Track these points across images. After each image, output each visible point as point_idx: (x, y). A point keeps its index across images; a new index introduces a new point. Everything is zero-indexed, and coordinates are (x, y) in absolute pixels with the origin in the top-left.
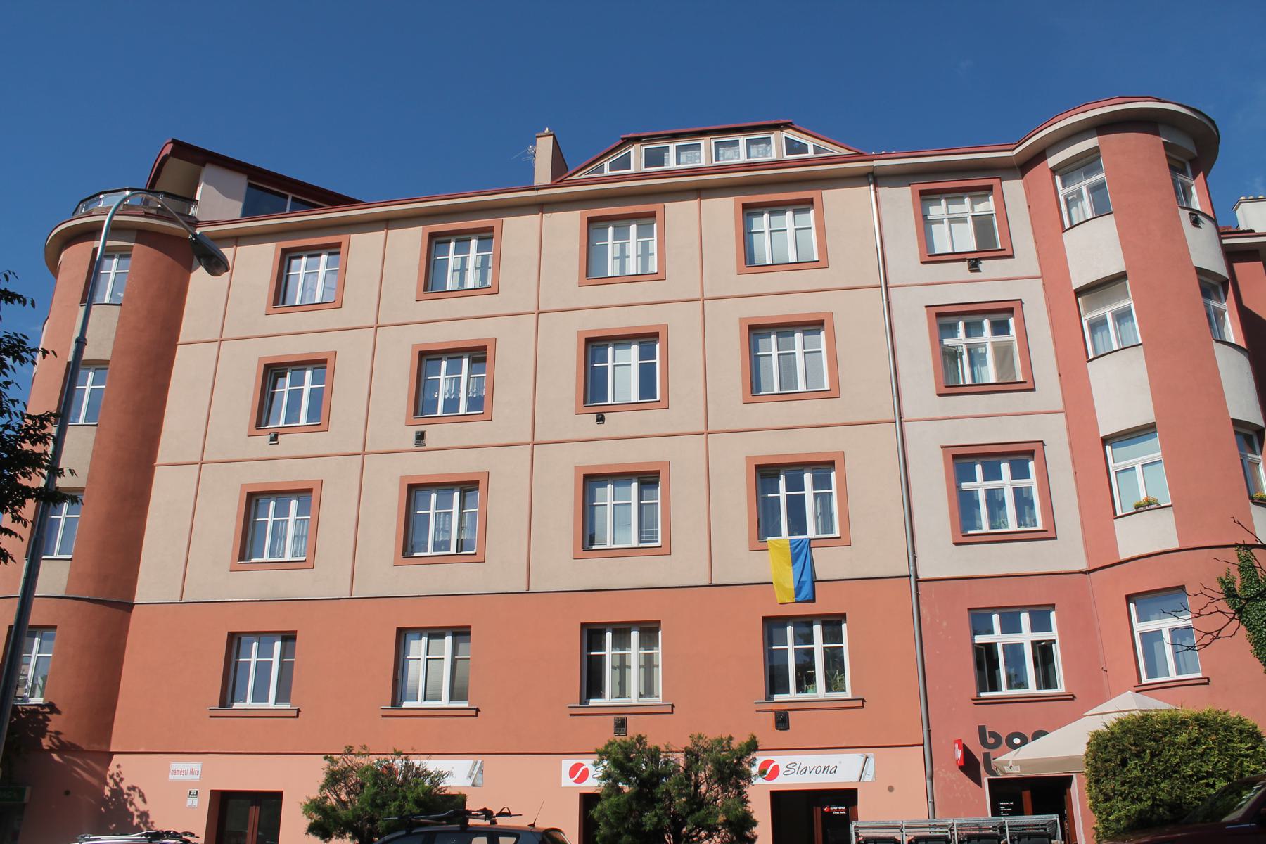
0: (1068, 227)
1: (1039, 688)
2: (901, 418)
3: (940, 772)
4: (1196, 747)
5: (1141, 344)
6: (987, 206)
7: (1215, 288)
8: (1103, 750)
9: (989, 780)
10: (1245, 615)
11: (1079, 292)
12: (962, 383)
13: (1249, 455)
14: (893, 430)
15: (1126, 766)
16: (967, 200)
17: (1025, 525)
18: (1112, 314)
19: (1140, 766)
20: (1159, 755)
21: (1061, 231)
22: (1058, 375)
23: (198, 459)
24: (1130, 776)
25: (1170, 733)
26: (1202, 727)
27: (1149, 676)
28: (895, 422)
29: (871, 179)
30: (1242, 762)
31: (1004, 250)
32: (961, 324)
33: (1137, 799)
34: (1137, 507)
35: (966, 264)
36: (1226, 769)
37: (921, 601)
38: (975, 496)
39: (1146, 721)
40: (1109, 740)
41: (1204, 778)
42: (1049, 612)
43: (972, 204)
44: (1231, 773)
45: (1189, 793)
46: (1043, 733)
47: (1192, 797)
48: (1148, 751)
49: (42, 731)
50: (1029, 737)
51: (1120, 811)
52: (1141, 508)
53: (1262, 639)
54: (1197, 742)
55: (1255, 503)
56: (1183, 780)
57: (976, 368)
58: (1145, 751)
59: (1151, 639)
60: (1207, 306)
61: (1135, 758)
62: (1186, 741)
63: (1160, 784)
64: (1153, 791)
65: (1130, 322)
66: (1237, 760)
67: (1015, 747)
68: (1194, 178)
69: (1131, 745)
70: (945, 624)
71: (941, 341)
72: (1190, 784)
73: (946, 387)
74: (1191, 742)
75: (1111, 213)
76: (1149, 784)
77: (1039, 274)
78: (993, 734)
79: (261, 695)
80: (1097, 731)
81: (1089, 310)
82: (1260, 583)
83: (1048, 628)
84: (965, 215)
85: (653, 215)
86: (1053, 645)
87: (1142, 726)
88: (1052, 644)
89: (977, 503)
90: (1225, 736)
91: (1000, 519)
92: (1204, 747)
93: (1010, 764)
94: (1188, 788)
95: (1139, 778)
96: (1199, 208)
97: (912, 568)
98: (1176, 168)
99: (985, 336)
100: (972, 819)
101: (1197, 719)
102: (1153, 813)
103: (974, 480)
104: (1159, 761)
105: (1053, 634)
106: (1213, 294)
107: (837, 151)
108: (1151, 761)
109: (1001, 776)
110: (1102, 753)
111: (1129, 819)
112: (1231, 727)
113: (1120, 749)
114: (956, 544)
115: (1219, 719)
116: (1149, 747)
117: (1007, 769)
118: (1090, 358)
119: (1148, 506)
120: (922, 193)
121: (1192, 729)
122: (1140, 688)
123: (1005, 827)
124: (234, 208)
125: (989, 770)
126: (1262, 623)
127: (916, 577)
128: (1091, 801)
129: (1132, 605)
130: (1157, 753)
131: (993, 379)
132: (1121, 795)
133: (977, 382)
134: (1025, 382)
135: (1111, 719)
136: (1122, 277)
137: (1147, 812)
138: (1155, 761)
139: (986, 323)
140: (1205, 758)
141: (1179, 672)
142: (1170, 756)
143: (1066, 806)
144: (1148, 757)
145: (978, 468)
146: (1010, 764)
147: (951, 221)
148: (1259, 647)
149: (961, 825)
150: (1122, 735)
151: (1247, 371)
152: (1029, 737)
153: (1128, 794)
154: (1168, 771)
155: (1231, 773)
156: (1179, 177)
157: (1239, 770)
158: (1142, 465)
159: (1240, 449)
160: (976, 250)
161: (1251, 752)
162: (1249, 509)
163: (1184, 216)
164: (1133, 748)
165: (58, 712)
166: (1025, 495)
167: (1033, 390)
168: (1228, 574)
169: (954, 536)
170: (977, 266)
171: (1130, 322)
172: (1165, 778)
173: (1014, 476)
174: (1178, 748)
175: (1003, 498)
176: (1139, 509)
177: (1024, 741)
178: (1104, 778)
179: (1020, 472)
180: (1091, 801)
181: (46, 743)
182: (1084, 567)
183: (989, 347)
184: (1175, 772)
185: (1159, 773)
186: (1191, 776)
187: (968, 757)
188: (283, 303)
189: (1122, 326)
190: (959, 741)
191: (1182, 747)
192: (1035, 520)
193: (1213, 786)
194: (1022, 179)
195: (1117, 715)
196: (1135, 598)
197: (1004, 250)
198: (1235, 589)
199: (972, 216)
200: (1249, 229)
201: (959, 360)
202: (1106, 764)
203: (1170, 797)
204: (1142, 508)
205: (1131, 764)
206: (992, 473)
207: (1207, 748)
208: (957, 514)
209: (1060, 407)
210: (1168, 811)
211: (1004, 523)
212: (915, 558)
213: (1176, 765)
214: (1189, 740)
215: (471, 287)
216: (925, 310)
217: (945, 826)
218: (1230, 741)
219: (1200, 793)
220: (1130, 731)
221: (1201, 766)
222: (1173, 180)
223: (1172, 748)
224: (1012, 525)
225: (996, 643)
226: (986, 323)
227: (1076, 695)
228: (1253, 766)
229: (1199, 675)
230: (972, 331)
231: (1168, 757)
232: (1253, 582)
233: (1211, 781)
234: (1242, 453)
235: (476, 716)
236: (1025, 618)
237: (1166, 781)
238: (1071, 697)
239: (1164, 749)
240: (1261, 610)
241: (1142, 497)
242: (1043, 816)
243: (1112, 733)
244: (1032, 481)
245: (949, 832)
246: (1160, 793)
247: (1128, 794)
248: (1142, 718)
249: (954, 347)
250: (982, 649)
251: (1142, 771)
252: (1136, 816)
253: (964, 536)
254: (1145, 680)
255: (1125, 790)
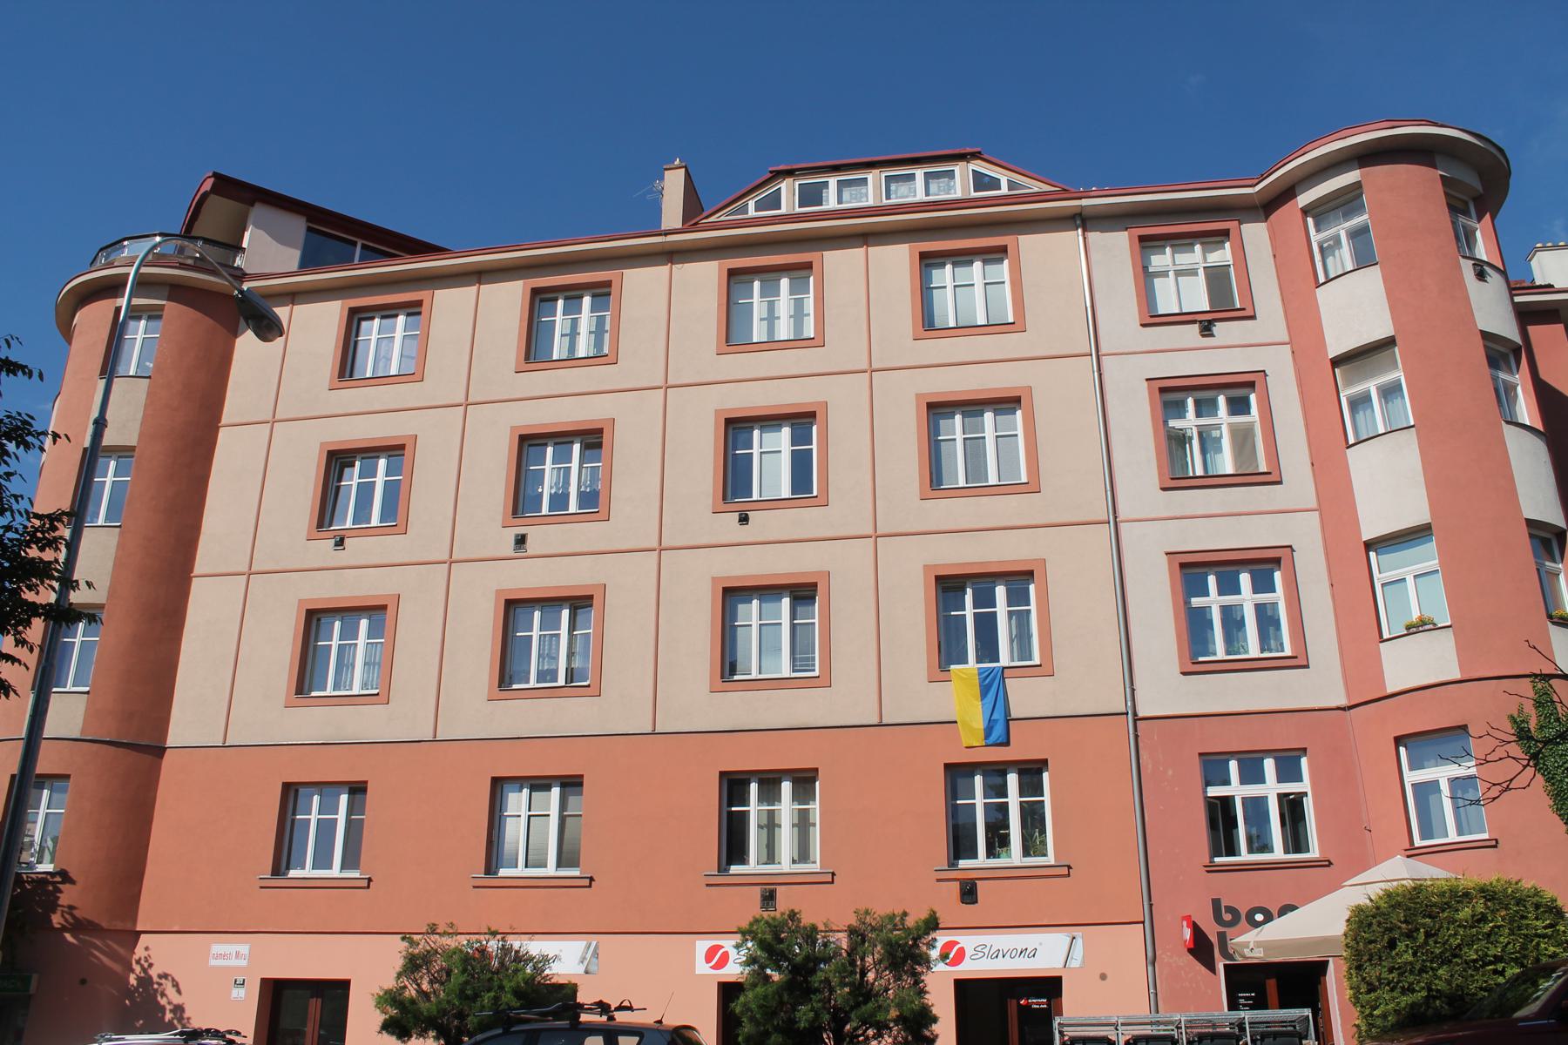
0: (1323, 281)
1: (1286, 851)
2: (1116, 517)
3: (1164, 956)
4: (1481, 925)
5: (1413, 426)
6: (1223, 255)
7: (1505, 357)
8: (1366, 929)
9: (1225, 966)
10: (1541, 761)
11: (1336, 362)
12: (1191, 475)
13: (1547, 563)
14: (1106, 532)
15: (1395, 948)
16: (1198, 248)
17: (1270, 650)
18: (1377, 388)
19: (1412, 948)
20: (1435, 934)
21: (1314, 286)
22: (1310, 465)
23: (245, 569)
24: (1400, 961)
25: (1450, 907)
26: (1489, 900)
27: (1423, 838)
28: (1109, 523)
29: (1078, 222)
30: (1538, 944)
31: (1244, 309)
32: (1190, 402)
33: (1408, 989)
34: (1408, 628)
35: (1196, 326)
36: (1519, 952)
37: (1140, 745)
38: (1208, 614)
39: (1419, 893)
40: (1374, 917)
41: (1491, 963)
42: (1300, 758)
43: (1204, 252)
44: (1525, 957)
45: (1473, 982)
46: (1292, 908)
47: (1476, 987)
48: (1422, 930)
49: (53, 906)
50: (1275, 913)
51: (1387, 1004)
52: (1414, 629)
53: (1563, 791)
54: (1483, 919)
55: (1554, 623)
56: (1465, 966)
57: (1208, 456)
58: (1419, 930)
59: (1426, 791)
60: (1495, 379)
61: (1406, 939)
62: (1469, 917)
63: (1437, 970)
64: (1427, 979)
65: (1399, 398)
66: (1532, 941)
67: (1257, 925)
68: (1479, 221)
69: (1401, 922)
70: (1170, 772)
71: (1165, 422)
72: (1474, 970)
73: (1172, 479)
74: (1476, 918)
75: (1377, 264)
76: (1423, 970)
77: (1287, 339)
78: (1230, 909)
79: (323, 860)
80: (1359, 905)
81: (1349, 383)
82: (1560, 722)
83: (1298, 778)
84: (1196, 266)
85: (808, 266)
86: (1305, 799)
87: (1415, 898)
88: (1302, 798)
89: (1211, 622)
90: (1517, 912)
91: (1238, 643)
92: (1491, 925)
93: (1251, 946)
94: (1472, 976)
95: (1411, 963)
96: (1485, 258)
97: (1129, 704)
98: (1456, 208)
99: (1220, 416)
100: (1204, 1014)
101: (1482, 890)
102: (1428, 1007)
103: (1207, 594)
104: (1436, 942)
105: (1305, 786)
106: (1502, 364)
107: (1036, 187)
108: (1426, 943)
109: (1240, 961)
110: (1365, 932)
111: (1398, 1014)
112: (1525, 901)
113: (1387, 927)
114: (1184, 674)
115: (1510, 891)
116: (1424, 925)
117: (1247, 952)
118: (1350, 443)
119: (1422, 626)
120: (1142, 239)
121: (1477, 903)
122: (1412, 852)
123: (1245, 1023)
124: (290, 257)
125: (1225, 954)
126: (1563, 771)
127: (1135, 714)
128: (1352, 992)
129: (1402, 750)
130: (1433, 932)
131: (1229, 470)
132: (1388, 984)
133: (1210, 473)
134: (1269, 473)
135: (1375, 891)
136: (1389, 342)
137: (1420, 1005)
138: (1431, 942)
139: (1222, 400)
140: (1493, 938)
141: (1460, 833)
142: (1449, 936)
143: (1320, 998)
144: (1421, 937)
145: (1212, 580)
146: (1251, 946)
147: (1178, 273)
148: (1560, 801)
149: (1190, 1021)
150: (1390, 910)
151: (1544, 460)
152: (1275, 913)
153: (1398, 983)
154: (1447, 955)
155: (1525, 957)
156: (1460, 219)
157: (1534, 954)
158: (1415, 576)
159: (1536, 556)
160: (1208, 309)
161: (1549, 931)
162: (1547, 630)
163: (1467, 267)
164: (1404, 926)
165: (72, 882)
166: (1269, 613)
167: (1280, 483)
168: (1520, 711)
169: (1181, 664)
170: (1210, 330)
171: (1399, 398)
172: (1443, 963)
173: (1256, 589)
174: (1459, 926)
175: (1243, 617)
176: (1411, 630)
177: (1269, 918)
178: (1367, 964)
179: (1263, 584)
180: (1352, 992)
181: (56, 919)
182: (1343, 702)
183: (1225, 429)
184: (1455, 956)
185: (1435, 957)
186: (1475, 961)
187: (1199, 937)
188: (351, 376)
189: (1390, 403)
190: (1188, 918)
191: (1463, 925)
192: (1282, 644)
193: (1502, 973)
194: (1266, 221)
195: (1383, 885)
196: (1406, 740)
197: (1244, 309)
198: (1529, 729)
199: (1204, 268)
200: (1547, 283)
201: (1187, 446)
202: (1370, 946)
203: (1449, 987)
204: (1415, 630)
205: (1401, 946)
206: (1229, 586)
207: (1495, 927)
208: (1185, 637)
209: (1313, 504)
210: (1446, 1004)
211: (1243, 647)
212: (1133, 690)
213: (1456, 948)
214: (1473, 916)
215: (583, 356)
216: (1146, 384)
217: (1171, 1023)
218: (1523, 917)
219: (1486, 982)
220: (1399, 905)
221: (1488, 948)
222: (1453, 223)
223: (1452, 927)
224: (1254, 650)
225: (1234, 796)
226: (1222, 400)
227: (1332, 861)
228: (1552, 949)
229: (1485, 836)
230: (1204, 409)
231: (1446, 938)
232: (1552, 721)
233: (1500, 967)
234: (1538, 561)
235: (590, 886)
236: (1269, 765)
237: (1445, 967)
238: (1327, 863)
239: (1441, 927)
240: (1562, 755)
241: (1415, 616)
242: (1292, 1011)
243: (1378, 908)
244: (1279, 596)
245: (1176, 1030)
246: (1437, 982)
247: (1398, 983)
248: (1415, 888)
249: (1181, 430)
250: (1217, 804)
251: (1415, 954)
252: (1407, 1010)
253: (1193, 663)
254: (1418, 842)
255: (1393, 978)
